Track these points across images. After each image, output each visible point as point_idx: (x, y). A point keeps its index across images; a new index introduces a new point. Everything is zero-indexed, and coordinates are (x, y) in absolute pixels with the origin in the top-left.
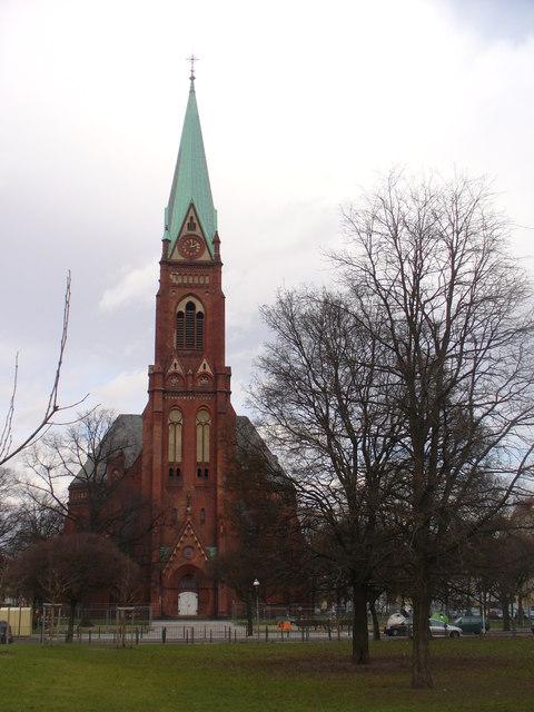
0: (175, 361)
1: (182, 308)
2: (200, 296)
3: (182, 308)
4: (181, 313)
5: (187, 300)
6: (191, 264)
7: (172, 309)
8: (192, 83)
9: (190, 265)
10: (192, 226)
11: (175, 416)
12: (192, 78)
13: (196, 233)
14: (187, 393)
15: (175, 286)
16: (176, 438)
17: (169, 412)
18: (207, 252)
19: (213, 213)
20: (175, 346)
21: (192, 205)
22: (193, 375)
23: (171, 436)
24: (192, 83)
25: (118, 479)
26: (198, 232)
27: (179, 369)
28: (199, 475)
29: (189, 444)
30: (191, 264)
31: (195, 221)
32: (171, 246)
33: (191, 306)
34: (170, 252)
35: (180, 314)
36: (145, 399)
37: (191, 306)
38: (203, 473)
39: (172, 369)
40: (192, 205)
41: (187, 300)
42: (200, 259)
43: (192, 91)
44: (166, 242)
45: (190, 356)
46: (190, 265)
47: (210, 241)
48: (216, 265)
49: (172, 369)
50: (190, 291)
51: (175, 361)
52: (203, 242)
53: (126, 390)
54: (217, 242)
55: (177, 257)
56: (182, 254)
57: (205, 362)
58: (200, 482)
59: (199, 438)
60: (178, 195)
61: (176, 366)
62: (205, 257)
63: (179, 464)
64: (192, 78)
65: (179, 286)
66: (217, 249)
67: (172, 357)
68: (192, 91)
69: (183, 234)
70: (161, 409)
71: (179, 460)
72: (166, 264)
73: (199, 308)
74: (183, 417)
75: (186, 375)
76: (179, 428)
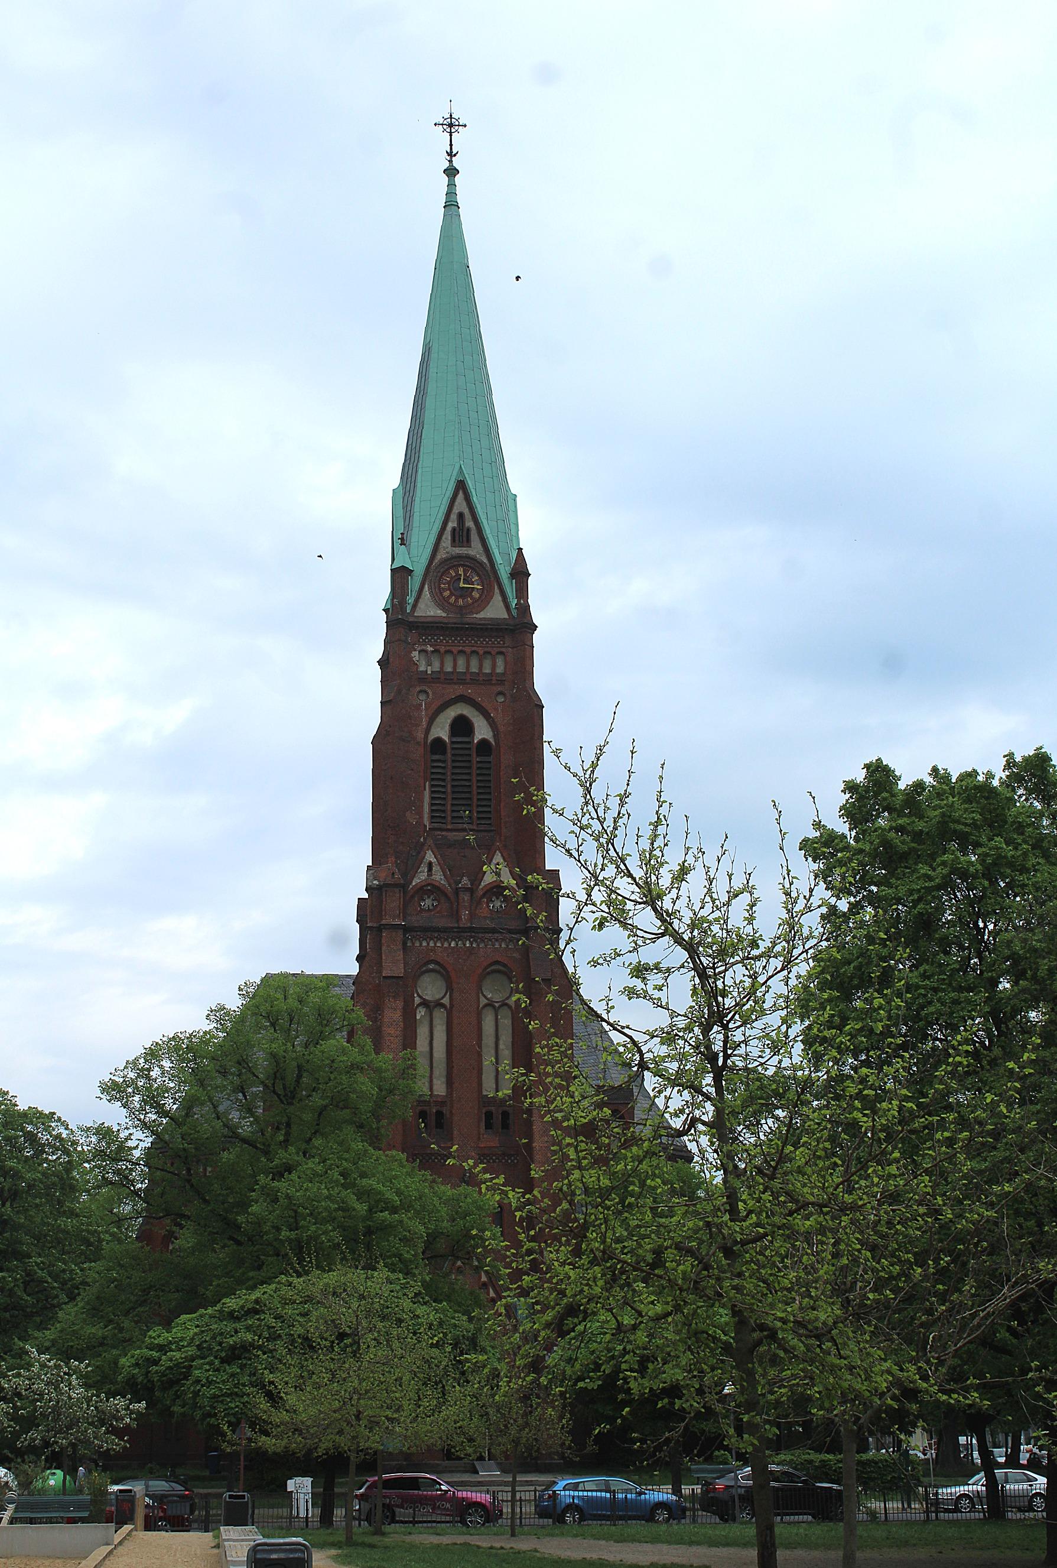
0: (430, 857)
1: (441, 731)
2: (487, 705)
3: (441, 731)
4: (438, 741)
5: (452, 713)
6: (458, 643)
7: (420, 735)
8: (451, 185)
9: (458, 631)
10: (461, 536)
11: (430, 988)
12: (451, 172)
13: (471, 552)
14: (460, 933)
15: (424, 679)
16: (433, 1038)
17: (416, 977)
18: (497, 597)
19: (508, 503)
20: (426, 822)
21: (461, 486)
22: (471, 891)
23: (422, 1032)
24: (451, 185)
25: (259, 1081)
26: (475, 550)
27: (438, 876)
28: (489, 1126)
29: (462, 1058)
30: (458, 643)
31: (469, 523)
32: (414, 583)
33: (462, 726)
34: (411, 600)
36: (347, 863)
37: (462, 726)
38: (497, 1120)
39: (421, 877)
40: (461, 486)
41: (452, 713)
42: (482, 615)
43: (451, 204)
44: (400, 575)
46: (458, 631)
47: (504, 572)
48: (520, 628)
49: (421, 877)
50: (460, 690)
51: (430, 857)
52: (487, 572)
53: (299, 901)
54: (521, 573)
55: (429, 609)
56: (441, 601)
57: (498, 858)
58: (491, 1141)
59: (488, 1039)
60: (425, 461)
61: (431, 869)
62: (495, 611)
63: (443, 1103)
64: (451, 172)
66: (522, 591)
67: (420, 849)
68: (451, 204)
69: (441, 555)
70: (399, 971)
71: (440, 1088)
72: (399, 619)
73: (482, 731)
74: (450, 988)
75: (457, 891)
76: (440, 1017)
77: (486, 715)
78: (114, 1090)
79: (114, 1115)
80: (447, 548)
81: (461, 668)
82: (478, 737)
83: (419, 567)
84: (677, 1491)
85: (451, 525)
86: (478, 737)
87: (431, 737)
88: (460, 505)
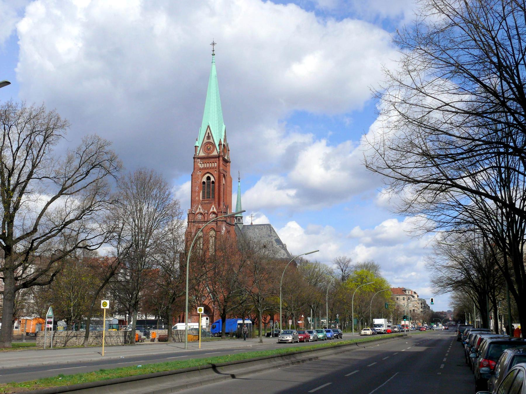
3: (204, 179)
7: (200, 181)
10: (209, 138)
15: (200, 169)
18: (215, 150)
21: (8, 83)
26: (211, 140)
31: (210, 135)
33: (208, 178)
34: (198, 152)
35: (204, 183)
37: (208, 178)
40: (209, 127)
45: (208, 203)
49: (211, 210)
56: (204, 151)
57: (213, 206)
65: (203, 169)
73: (212, 179)
77: (213, 175)
78: (338, 263)
79: (335, 266)
80: (206, 140)
81: (208, 166)
82: (211, 180)
83: (200, 145)
84: (244, 321)
85: (207, 135)
86: (211, 180)
87: (202, 181)
88: (208, 131)
